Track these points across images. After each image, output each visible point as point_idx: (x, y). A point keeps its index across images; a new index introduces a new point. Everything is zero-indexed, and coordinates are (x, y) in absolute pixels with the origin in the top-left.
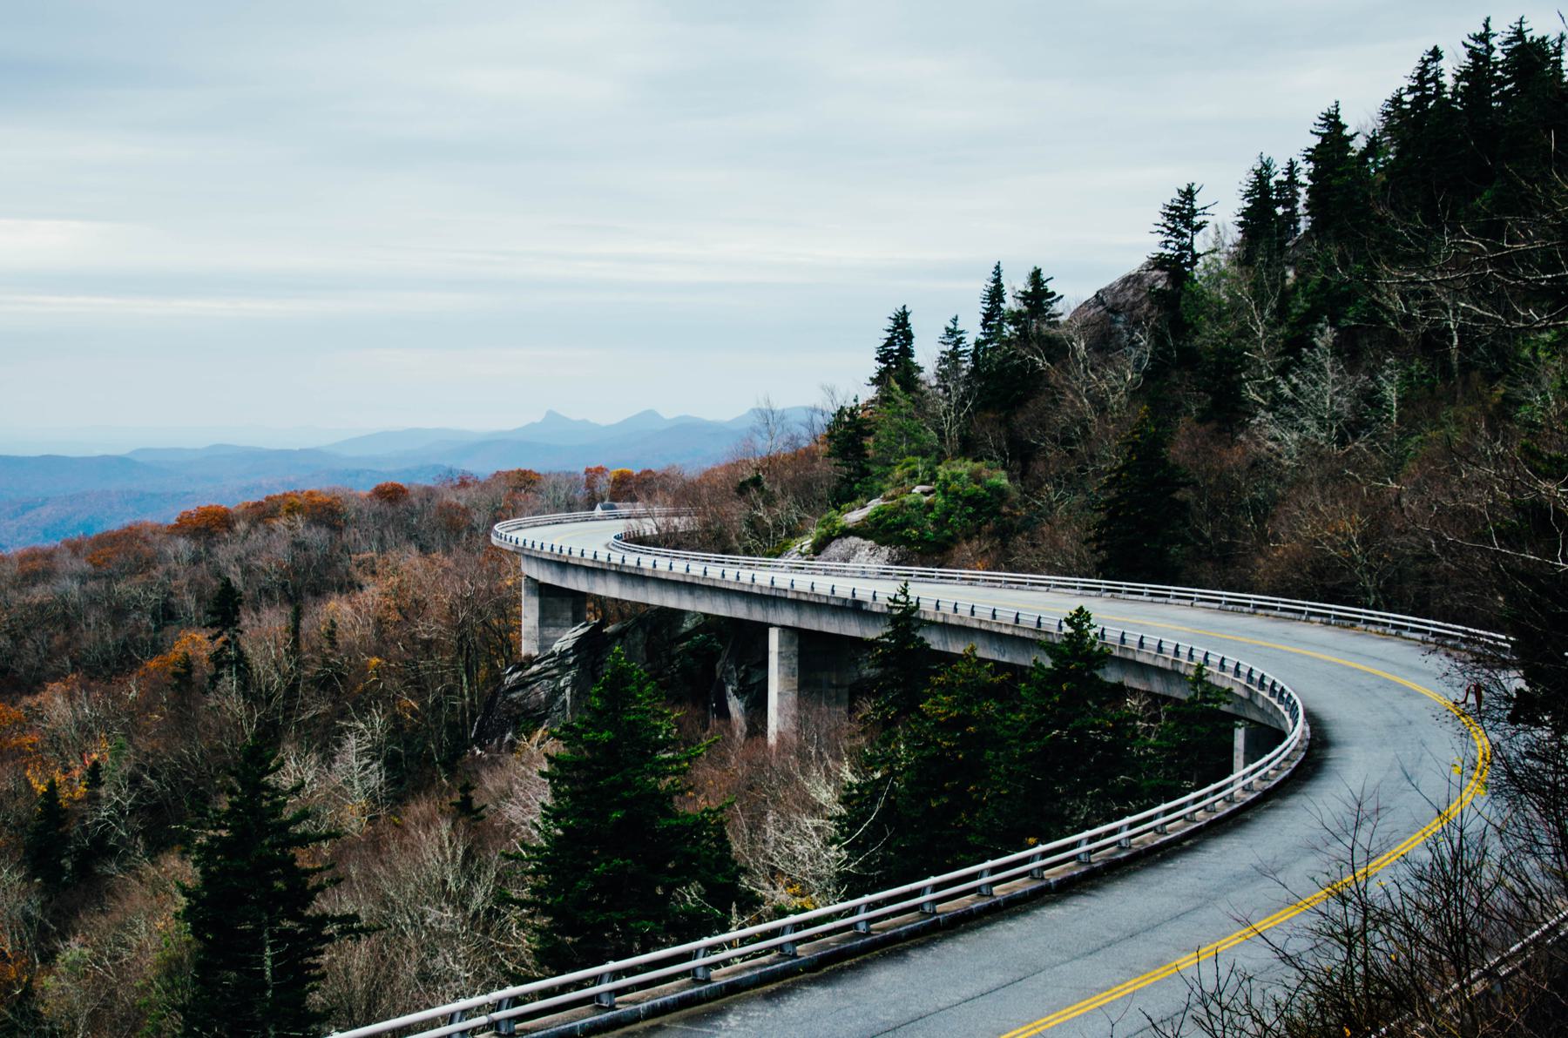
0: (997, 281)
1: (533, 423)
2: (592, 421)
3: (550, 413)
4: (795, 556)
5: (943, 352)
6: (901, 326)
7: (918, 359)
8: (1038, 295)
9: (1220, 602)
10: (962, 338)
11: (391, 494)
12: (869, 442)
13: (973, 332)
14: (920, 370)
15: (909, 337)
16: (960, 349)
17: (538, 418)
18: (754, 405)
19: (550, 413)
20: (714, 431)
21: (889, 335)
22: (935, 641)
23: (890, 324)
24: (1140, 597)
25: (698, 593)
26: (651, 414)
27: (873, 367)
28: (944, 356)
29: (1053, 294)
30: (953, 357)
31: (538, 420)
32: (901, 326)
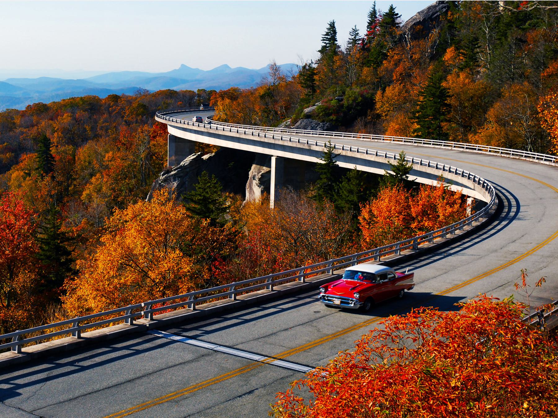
0: (374, 8)
1: (175, 70)
2: (200, 69)
3: (182, 65)
4: (283, 126)
5: (350, 39)
6: (332, 31)
7: (339, 43)
8: (391, 15)
9: (370, 138)
10: (358, 33)
11: (115, 98)
12: (316, 77)
13: (363, 32)
14: (339, 47)
15: (335, 32)
16: (357, 38)
17: (177, 67)
18: (269, 63)
19: (182, 65)
20: (251, 74)
21: (327, 31)
22: (341, 164)
23: (329, 27)
24: (474, 151)
25: (186, 364)
26: (226, 66)
27: (320, 45)
28: (349, 40)
29: (397, 14)
30: (355, 41)
31: (177, 68)
32: (332, 31)
